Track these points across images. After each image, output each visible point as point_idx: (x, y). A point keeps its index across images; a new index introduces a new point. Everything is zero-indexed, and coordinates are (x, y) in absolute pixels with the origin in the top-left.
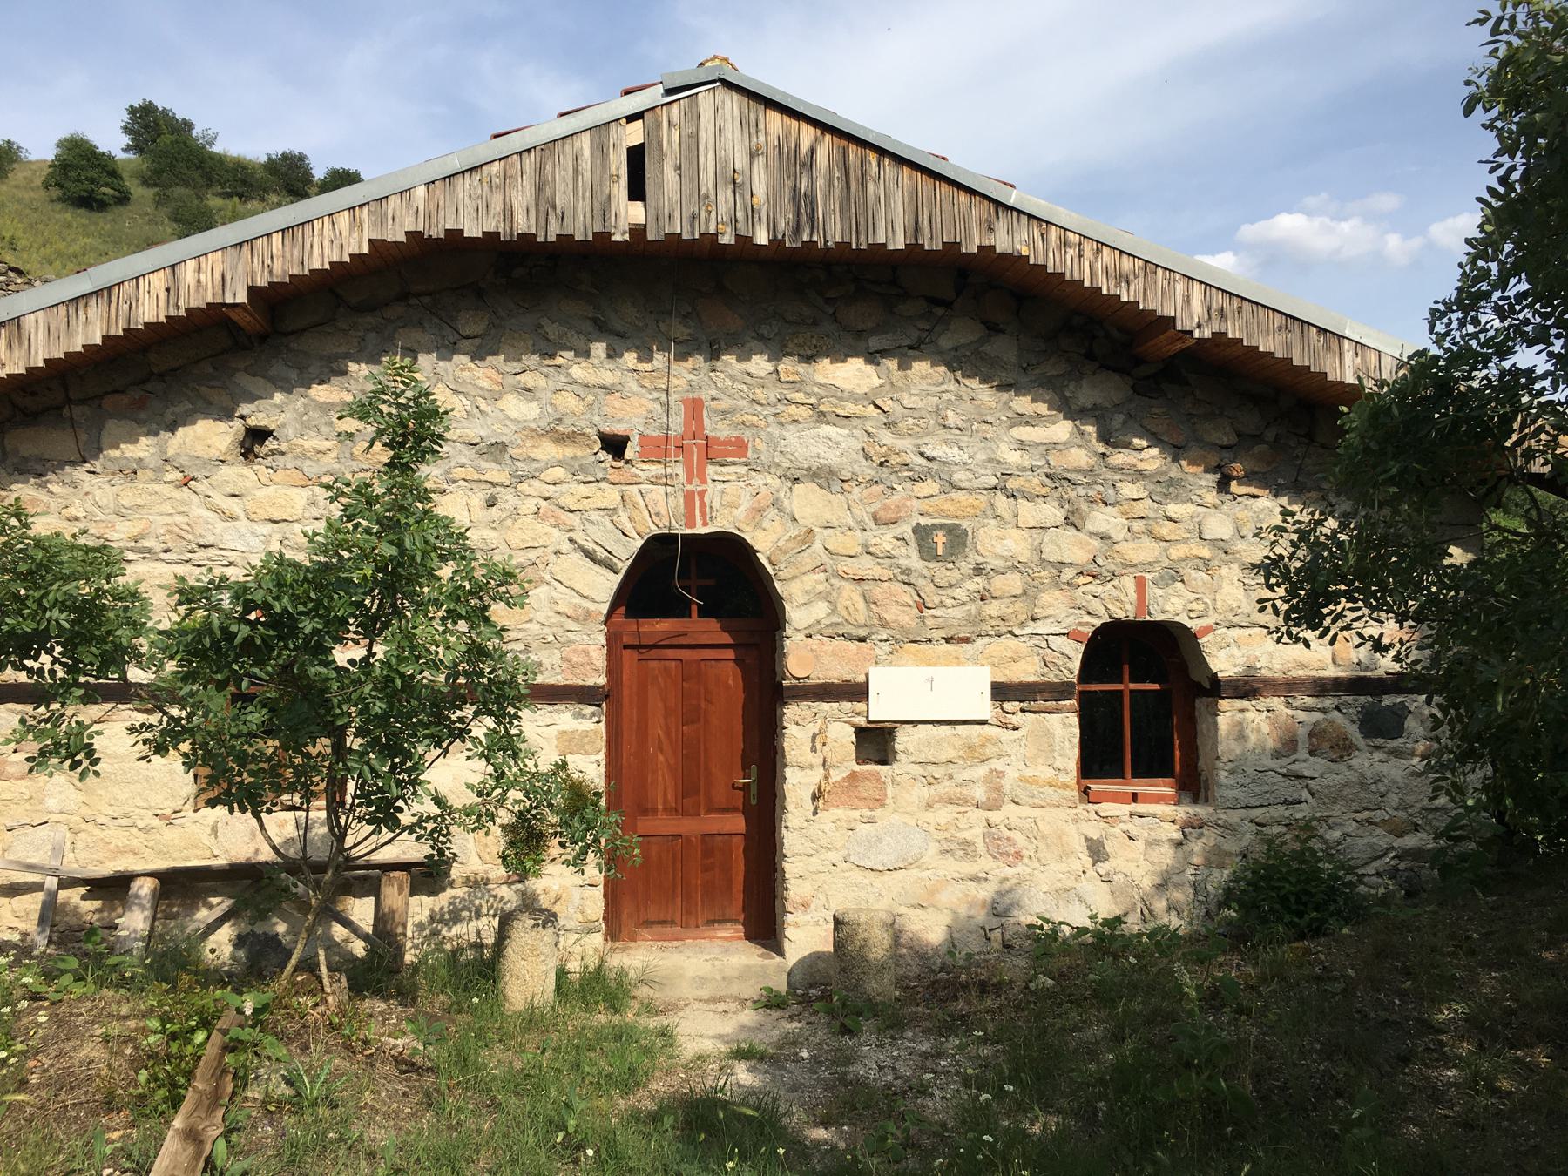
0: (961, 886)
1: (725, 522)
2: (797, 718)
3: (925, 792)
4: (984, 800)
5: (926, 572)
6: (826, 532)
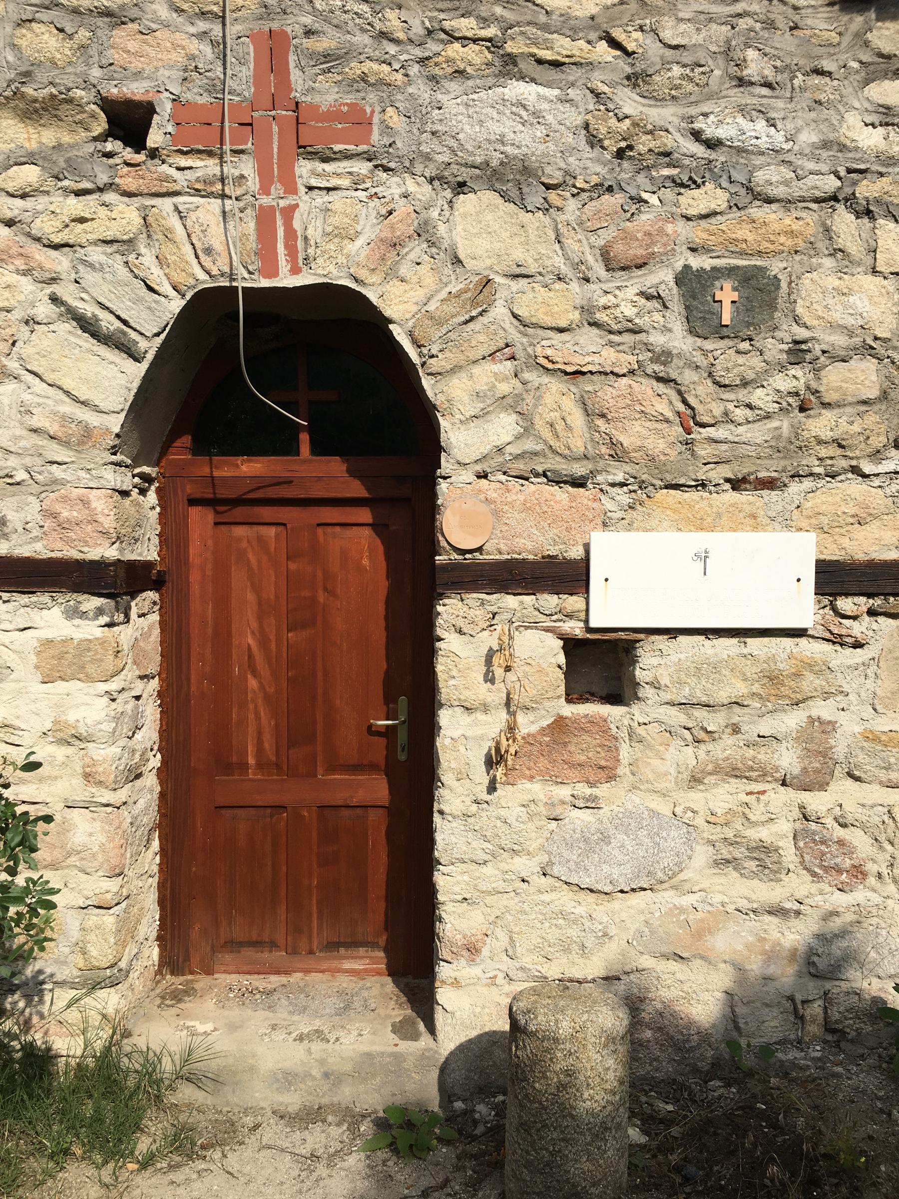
0: (752, 924)
1: (332, 268)
2: (460, 623)
3: (689, 756)
4: (796, 771)
5: (699, 358)
6: (517, 285)
